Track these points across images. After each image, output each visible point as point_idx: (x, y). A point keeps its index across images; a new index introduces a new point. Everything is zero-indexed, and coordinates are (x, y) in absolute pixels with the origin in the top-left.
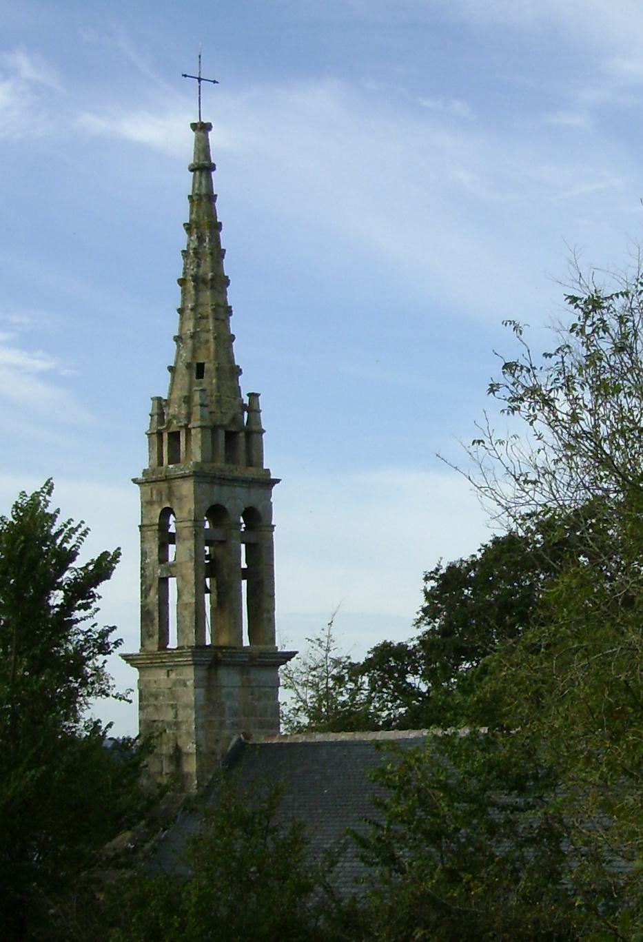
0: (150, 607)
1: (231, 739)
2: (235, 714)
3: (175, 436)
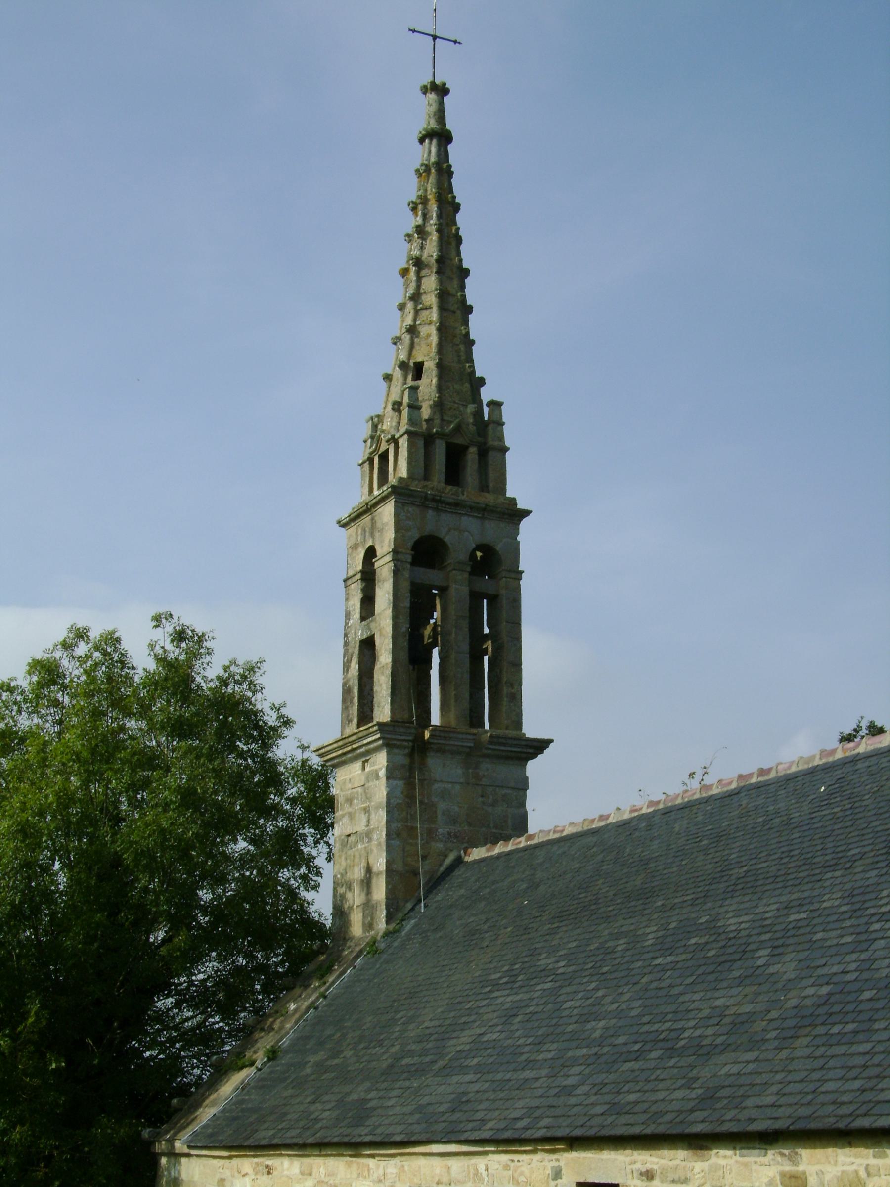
0: (351, 683)
1: (446, 856)
2: (454, 821)
3: (384, 457)
